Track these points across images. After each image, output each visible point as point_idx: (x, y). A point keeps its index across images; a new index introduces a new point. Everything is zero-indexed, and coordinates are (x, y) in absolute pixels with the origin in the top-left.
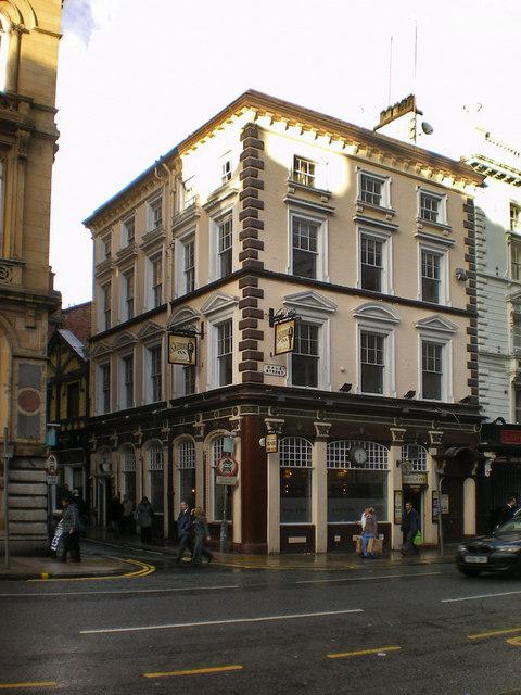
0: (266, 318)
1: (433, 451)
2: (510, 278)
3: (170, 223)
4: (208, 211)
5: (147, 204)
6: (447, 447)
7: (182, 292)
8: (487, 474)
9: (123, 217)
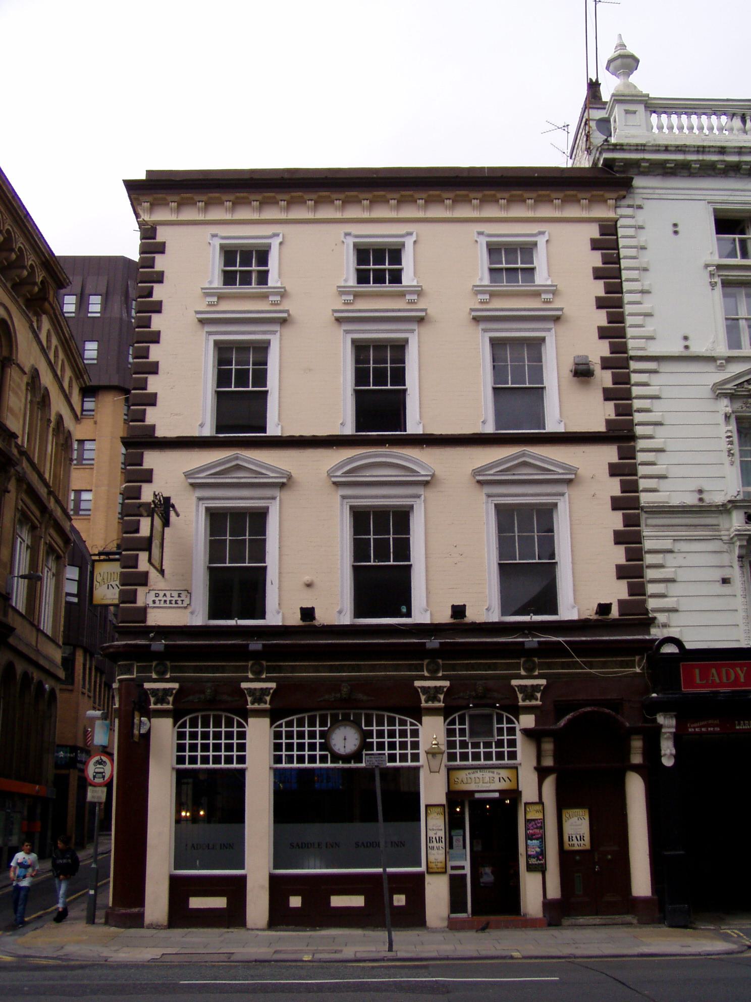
1: (528, 721)
8: (668, 762)
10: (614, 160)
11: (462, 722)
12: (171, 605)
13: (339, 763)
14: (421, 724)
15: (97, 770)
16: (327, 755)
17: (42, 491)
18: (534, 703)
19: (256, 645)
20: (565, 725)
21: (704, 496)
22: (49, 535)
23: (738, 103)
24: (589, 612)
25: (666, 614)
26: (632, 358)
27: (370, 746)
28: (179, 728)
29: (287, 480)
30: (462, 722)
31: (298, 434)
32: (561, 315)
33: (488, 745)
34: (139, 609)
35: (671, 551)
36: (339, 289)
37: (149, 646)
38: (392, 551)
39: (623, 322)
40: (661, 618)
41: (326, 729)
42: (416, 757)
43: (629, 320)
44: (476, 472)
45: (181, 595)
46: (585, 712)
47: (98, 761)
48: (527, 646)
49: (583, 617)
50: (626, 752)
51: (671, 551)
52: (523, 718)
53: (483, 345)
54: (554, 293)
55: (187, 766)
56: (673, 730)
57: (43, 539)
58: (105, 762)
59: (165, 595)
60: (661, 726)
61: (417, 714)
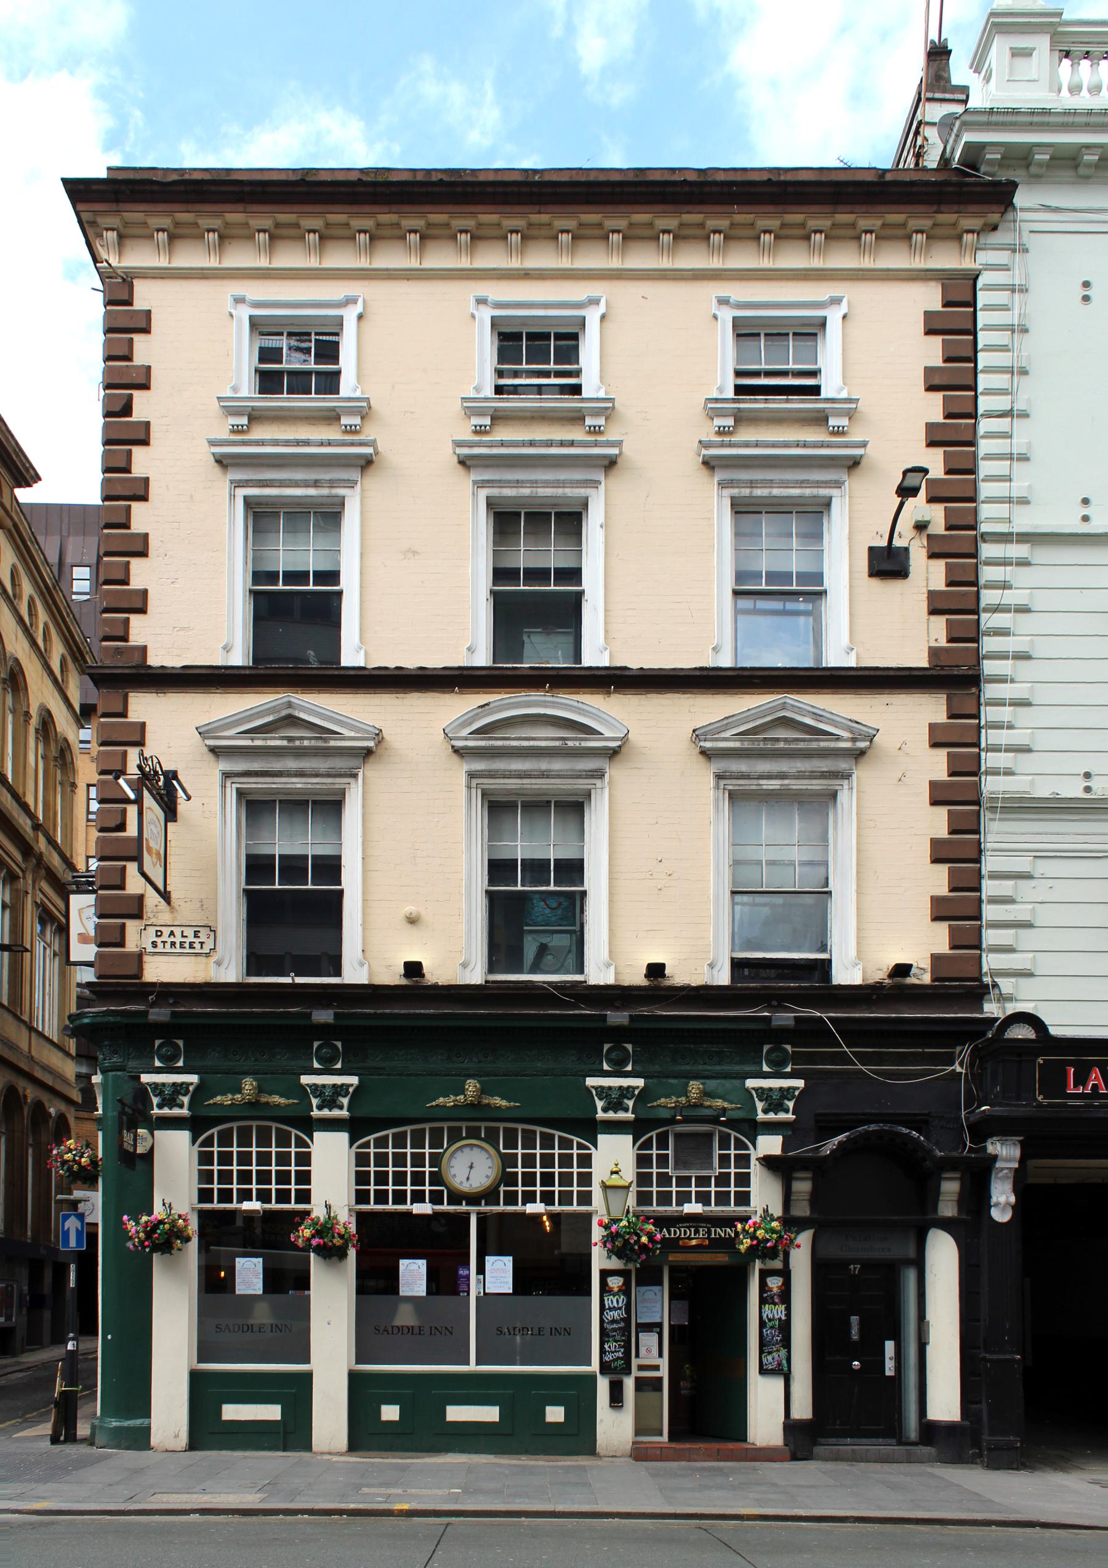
8: (1001, 1215)
10: (981, 147)
11: (663, 1143)
13: (461, 1204)
14: (596, 1148)
16: (443, 1191)
17: (21, 821)
18: (782, 1116)
19: (323, 1016)
20: (833, 1151)
22: (40, 890)
24: (879, 973)
25: (1013, 980)
26: (986, 537)
27: (511, 1180)
28: (201, 1145)
29: (376, 745)
30: (663, 1143)
31: (392, 665)
32: (861, 456)
33: (703, 1181)
35: (1027, 876)
36: (465, 404)
37: (145, 1014)
38: (552, 868)
39: (972, 471)
40: (1006, 985)
41: (441, 1151)
42: (586, 1198)
43: (985, 468)
44: (697, 735)
45: (199, 935)
46: (867, 1132)
48: (775, 1023)
49: (870, 981)
50: (928, 1197)
51: (1027, 876)
52: (762, 1140)
53: (720, 517)
54: (850, 414)
55: (216, 1205)
56: (1016, 1165)
57: (29, 896)
59: (172, 933)
60: (995, 1158)
61: (590, 1129)
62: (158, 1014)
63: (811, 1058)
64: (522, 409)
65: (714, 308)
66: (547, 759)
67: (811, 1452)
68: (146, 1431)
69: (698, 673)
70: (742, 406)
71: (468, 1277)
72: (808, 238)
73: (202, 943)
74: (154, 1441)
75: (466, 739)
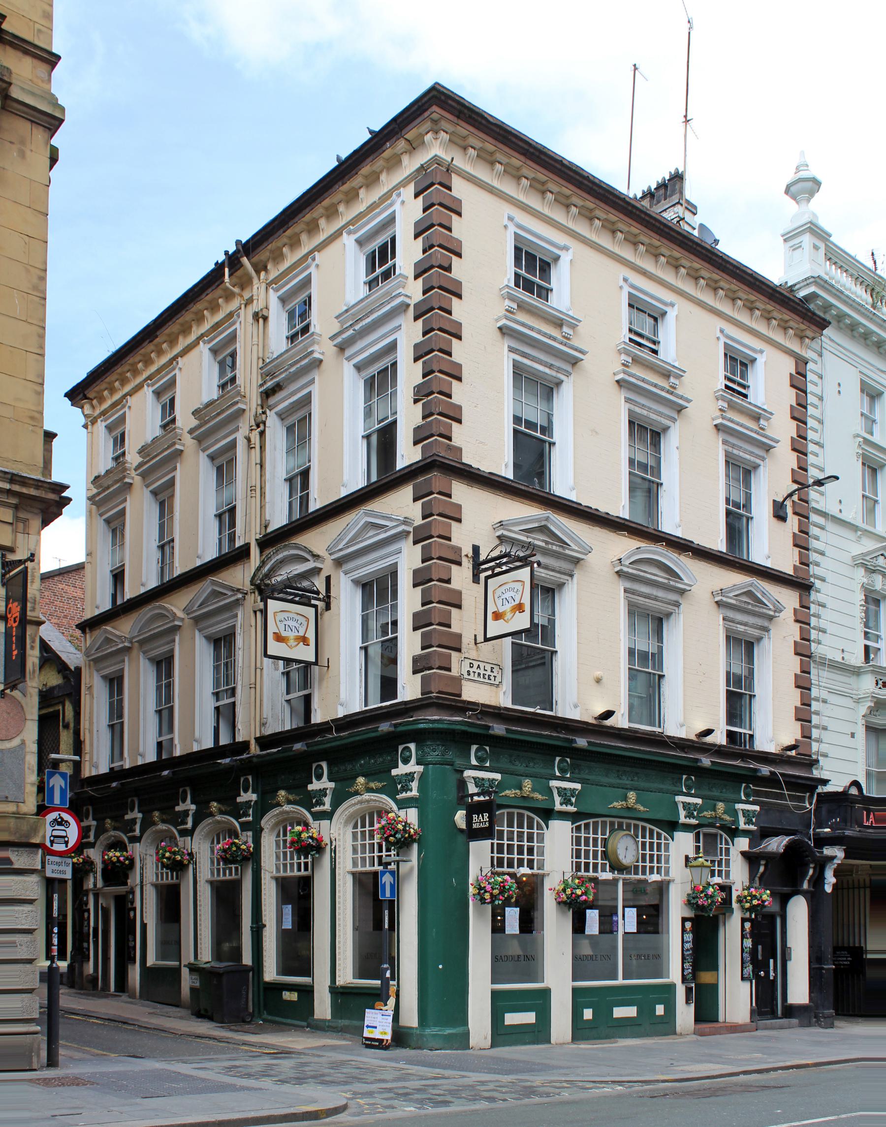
0: (467, 564)
1: (743, 844)
2: (859, 522)
3: (256, 380)
4: (342, 348)
5: (204, 349)
6: (765, 833)
7: (279, 519)
8: (828, 889)
9: (149, 378)
12: (489, 681)
15: (56, 833)
21: (846, 655)
23: (824, 235)
34: (453, 678)
47: (55, 820)
58: (67, 821)
59: (479, 667)
62: (499, 729)
63: (767, 795)
64: (646, 360)
65: (506, 221)
66: (656, 589)
67: (833, 1023)
68: (467, 1035)
69: (719, 554)
70: (734, 399)
71: (617, 922)
72: (465, 148)
73: (495, 677)
74: (472, 1043)
75: (731, 598)
